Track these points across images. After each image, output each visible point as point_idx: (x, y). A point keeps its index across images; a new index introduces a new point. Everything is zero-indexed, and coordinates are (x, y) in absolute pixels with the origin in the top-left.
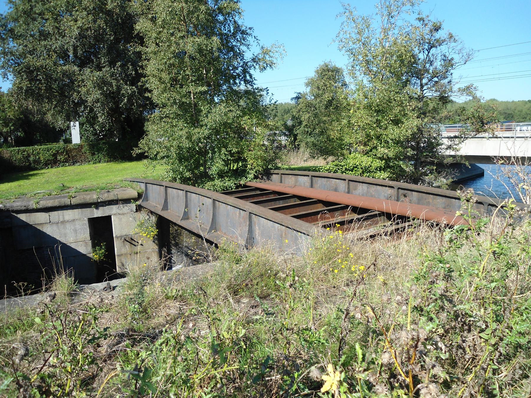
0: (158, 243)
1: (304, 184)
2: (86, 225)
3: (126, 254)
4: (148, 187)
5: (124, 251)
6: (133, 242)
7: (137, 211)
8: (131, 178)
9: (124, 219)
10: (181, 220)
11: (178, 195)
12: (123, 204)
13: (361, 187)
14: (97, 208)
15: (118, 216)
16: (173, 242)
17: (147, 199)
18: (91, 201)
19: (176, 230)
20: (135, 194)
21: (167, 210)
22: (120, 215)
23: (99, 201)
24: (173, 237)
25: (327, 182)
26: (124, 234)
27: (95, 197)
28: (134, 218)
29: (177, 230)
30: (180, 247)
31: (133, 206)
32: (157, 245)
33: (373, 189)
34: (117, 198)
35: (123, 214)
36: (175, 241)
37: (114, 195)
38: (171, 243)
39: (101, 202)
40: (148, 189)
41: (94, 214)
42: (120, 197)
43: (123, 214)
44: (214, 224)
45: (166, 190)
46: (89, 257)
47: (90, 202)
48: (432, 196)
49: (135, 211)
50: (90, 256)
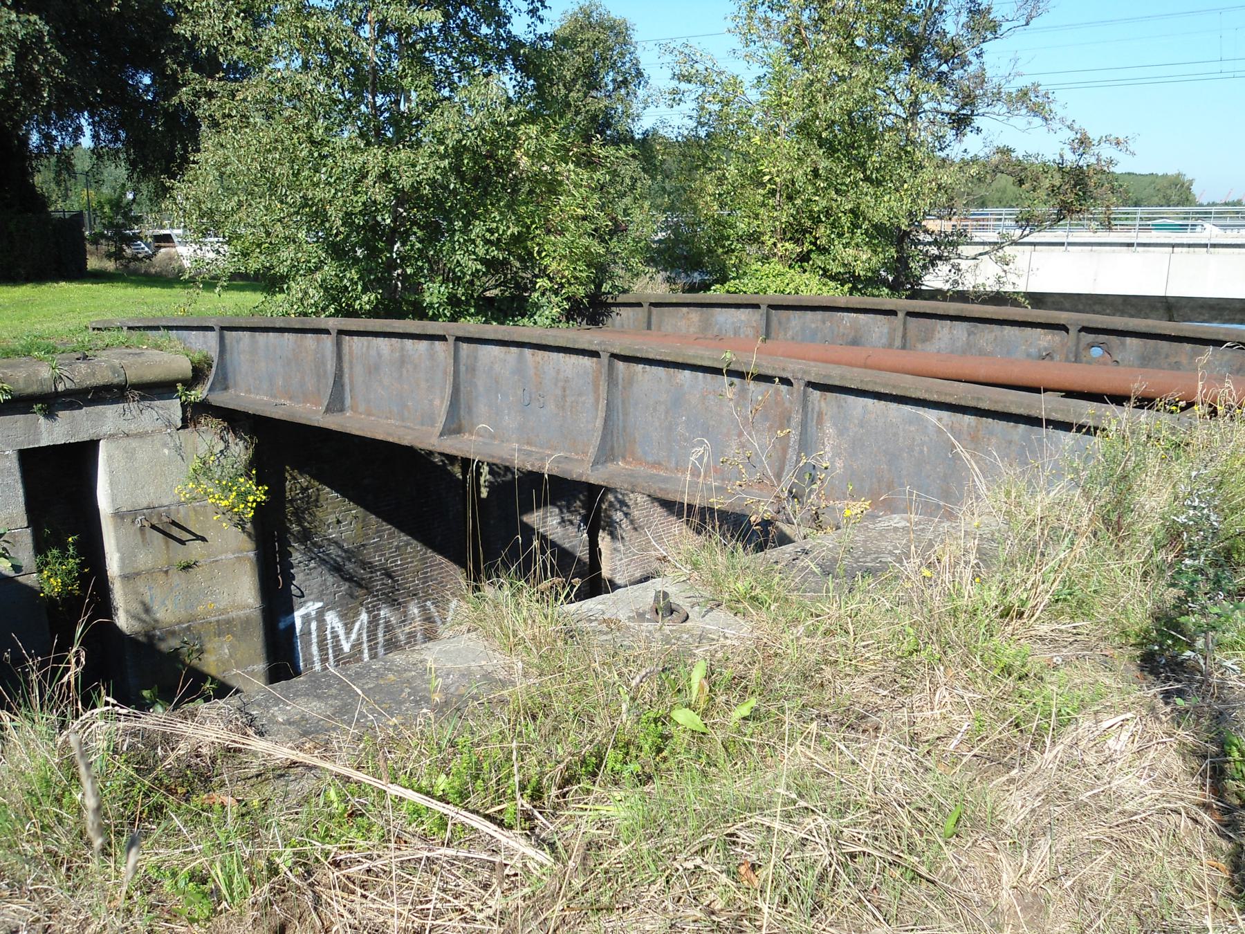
0: (252, 531)
1: (736, 331)
2: (10, 474)
3: (150, 572)
4: (227, 341)
5: (144, 560)
6: (175, 532)
7: (184, 426)
8: (130, 319)
9: (143, 451)
10: (441, 435)
11: (402, 356)
12: (143, 398)
13: (946, 331)
14: (50, 414)
15: (124, 442)
16: (295, 528)
17: (223, 382)
18: (34, 389)
19: (304, 490)
20: (181, 366)
21: (342, 410)
22: (130, 440)
23: (61, 388)
24: (295, 514)
25: (824, 323)
26: (145, 505)
27: (45, 373)
28: (178, 449)
29: (307, 488)
30: (315, 544)
31: (174, 409)
32: (249, 535)
33: (991, 337)
34: (122, 378)
35: (141, 436)
36: (300, 524)
37: (114, 370)
38: (288, 530)
39: (68, 393)
40: (228, 347)
41: (37, 433)
42: (133, 376)
43: (141, 436)
44: (609, 437)
45: (339, 345)
46: (26, 586)
47: (30, 391)
48: (1188, 347)
49: (180, 425)
50: (29, 583)
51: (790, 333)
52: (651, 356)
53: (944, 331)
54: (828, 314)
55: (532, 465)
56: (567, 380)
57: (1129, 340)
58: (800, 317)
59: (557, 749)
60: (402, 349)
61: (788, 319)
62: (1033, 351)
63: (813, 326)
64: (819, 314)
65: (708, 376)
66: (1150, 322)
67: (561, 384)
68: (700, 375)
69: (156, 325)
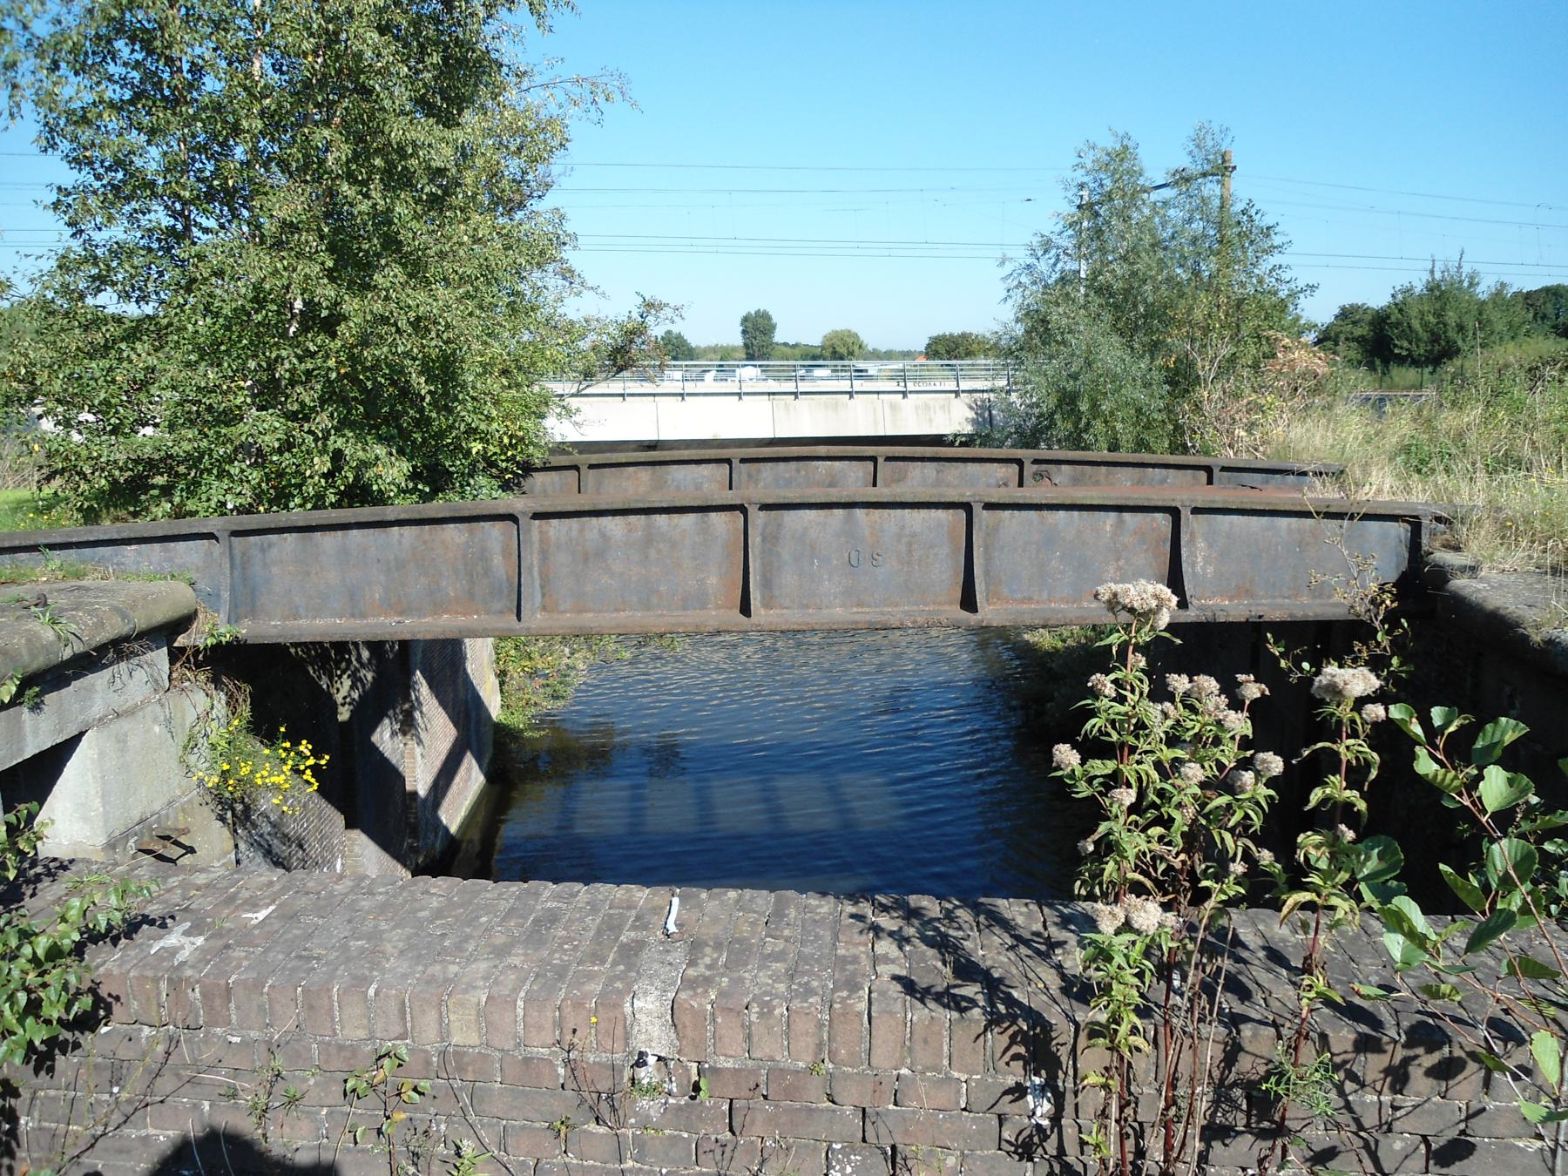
25: (798, 471)
48: (1103, 469)
53: (916, 469)
54: (801, 464)
56: (914, 535)
57: (1064, 467)
59: (795, 919)
61: (759, 471)
62: (992, 481)
64: (793, 465)
65: (1085, 514)
67: (904, 540)
68: (1076, 513)
69: (32, 543)
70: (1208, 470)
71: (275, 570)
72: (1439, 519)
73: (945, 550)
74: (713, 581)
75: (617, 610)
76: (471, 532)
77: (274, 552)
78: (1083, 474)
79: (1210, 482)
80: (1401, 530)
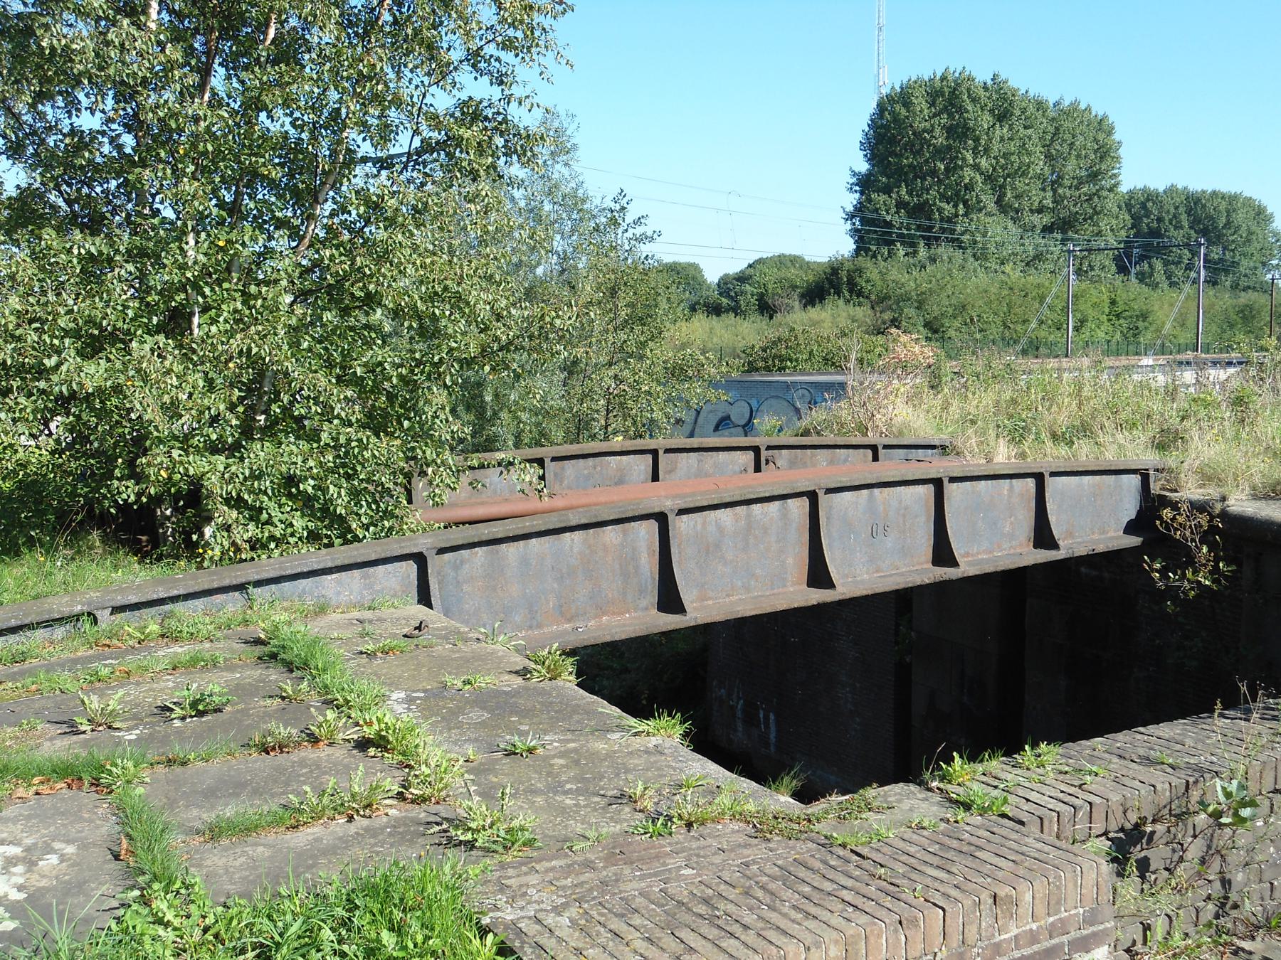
51: (566, 482)
52: (728, 500)
55: (929, 579)
58: (573, 466)
60: (749, 516)
61: (563, 469)
63: (586, 472)
64: (590, 461)
66: (736, 439)
70: (874, 448)
71: (466, 588)
72: (1158, 470)
73: (922, 519)
74: (790, 561)
75: (728, 595)
76: (625, 533)
77: (466, 569)
78: (796, 457)
79: (875, 458)
80: (1135, 480)
